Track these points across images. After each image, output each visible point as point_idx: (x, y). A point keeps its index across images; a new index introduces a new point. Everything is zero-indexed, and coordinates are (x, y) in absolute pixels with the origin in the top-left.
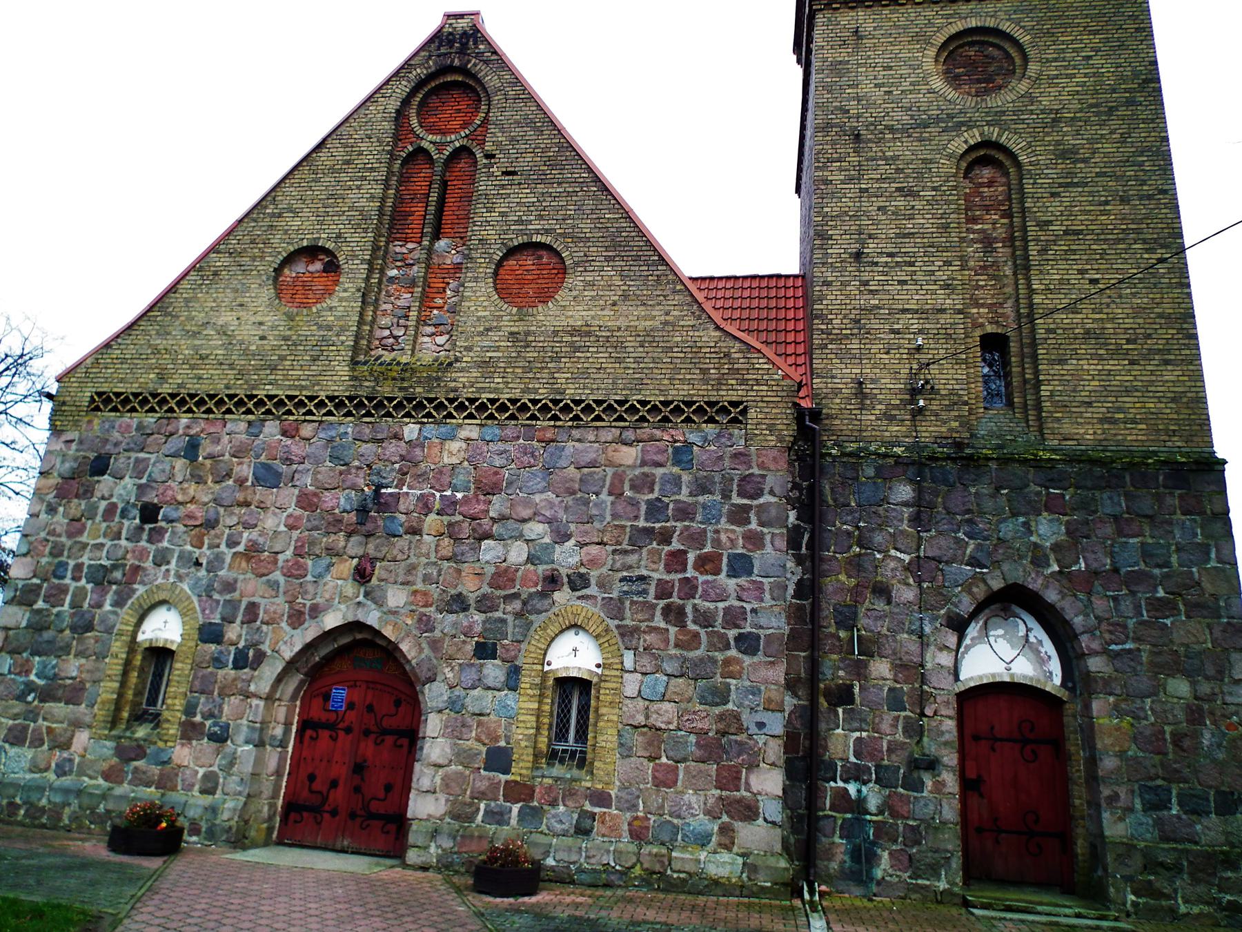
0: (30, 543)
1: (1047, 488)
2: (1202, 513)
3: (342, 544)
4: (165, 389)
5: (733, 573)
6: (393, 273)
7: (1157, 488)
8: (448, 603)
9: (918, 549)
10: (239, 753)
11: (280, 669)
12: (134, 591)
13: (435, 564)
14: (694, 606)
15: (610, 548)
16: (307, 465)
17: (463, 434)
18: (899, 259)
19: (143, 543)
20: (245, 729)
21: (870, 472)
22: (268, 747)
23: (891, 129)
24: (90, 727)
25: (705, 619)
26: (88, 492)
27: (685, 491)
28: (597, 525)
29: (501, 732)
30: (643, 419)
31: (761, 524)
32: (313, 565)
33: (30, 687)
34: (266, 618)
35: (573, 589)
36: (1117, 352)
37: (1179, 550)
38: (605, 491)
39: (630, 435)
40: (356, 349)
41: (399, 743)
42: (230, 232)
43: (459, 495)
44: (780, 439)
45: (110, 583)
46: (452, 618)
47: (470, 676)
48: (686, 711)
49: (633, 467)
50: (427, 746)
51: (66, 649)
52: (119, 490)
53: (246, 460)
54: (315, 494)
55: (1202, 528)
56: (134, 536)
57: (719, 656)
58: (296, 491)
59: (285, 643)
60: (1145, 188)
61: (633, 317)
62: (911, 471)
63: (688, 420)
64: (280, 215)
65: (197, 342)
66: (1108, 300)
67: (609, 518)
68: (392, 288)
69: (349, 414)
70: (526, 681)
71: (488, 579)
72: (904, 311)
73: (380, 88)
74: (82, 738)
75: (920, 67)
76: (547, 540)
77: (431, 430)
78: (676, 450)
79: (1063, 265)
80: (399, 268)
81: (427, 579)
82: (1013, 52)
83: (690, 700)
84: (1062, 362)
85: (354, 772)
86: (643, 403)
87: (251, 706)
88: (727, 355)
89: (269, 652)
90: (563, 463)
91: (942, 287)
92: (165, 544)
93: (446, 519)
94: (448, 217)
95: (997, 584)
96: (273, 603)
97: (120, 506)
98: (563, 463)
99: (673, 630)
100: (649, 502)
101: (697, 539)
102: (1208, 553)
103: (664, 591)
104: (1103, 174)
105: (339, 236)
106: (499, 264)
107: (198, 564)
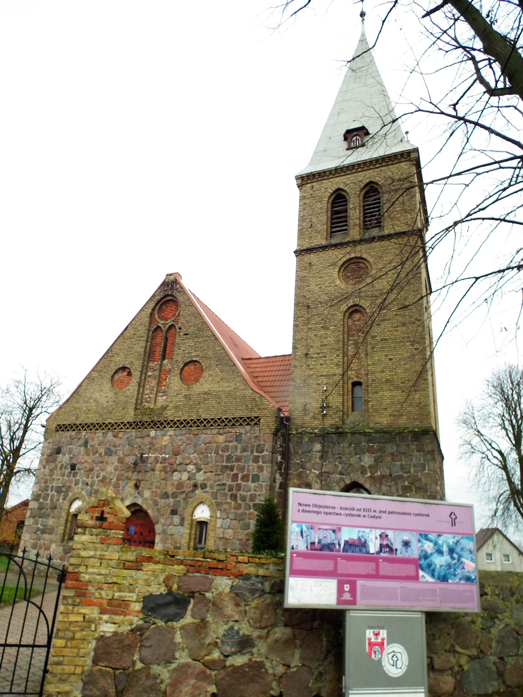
0: (38, 479)
1: (368, 443)
2: (424, 451)
3: (131, 475)
4: (78, 422)
5: (253, 482)
6: (150, 374)
7: (408, 442)
8: (163, 495)
9: (322, 468)
12: (68, 495)
13: (159, 481)
14: (240, 494)
15: (214, 474)
16: (121, 447)
17: (169, 433)
18: (321, 355)
19: (71, 478)
21: (306, 439)
23: (321, 303)
24: (56, 542)
25: (243, 499)
26: (55, 461)
27: (239, 451)
28: (210, 465)
29: (178, 541)
30: (226, 425)
31: (263, 462)
33: (38, 529)
35: (202, 489)
36: (397, 388)
37: (414, 466)
38: (213, 452)
39: (222, 431)
40: (136, 404)
42: (98, 364)
43: (167, 456)
44: (271, 430)
45: (62, 492)
46: (164, 501)
47: (169, 521)
48: (236, 532)
49: (222, 443)
51: (49, 516)
52: (64, 459)
53: (102, 447)
54: (123, 458)
55: (423, 457)
56: (68, 476)
57: (247, 512)
58: (117, 457)
60: (412, 319)
61: (226, 387)
62: (321, 438)
63: (241, 424)
64: (113, 356)
65: (88, 405)
66: (395, 367)
67: (214, 462)
68: (150, 379)
69: (134, 428)
70: (187, 523)
71: (175, 486)
72: (322, 376)
73: (145, 305)
74: (53, 546)
75: (332, 276)
76: (194, 471)
77: (159, 433)
78: (237, 436)
79: (379, 353)
80: (152, 372)
81: (157, 487)
82: (368, 265)
83: (237, 528)
84: (377, 393)
86: (226, 419)
88: (254, 399)
90: (200, 443)
91: (336, 366)
92: (78, 478)
93: (163, 465)
94: (167, 352)
95: (348, 482)
97: (65, 465)
98: (200, 443)
99: (233, 503)
100: (227, 456)
101: (242, 469)
102: (425, 467)
103: (231, 489)
104: (396, 315)
105: (131, 362)
106: (182, 369)
107: (87, 484)
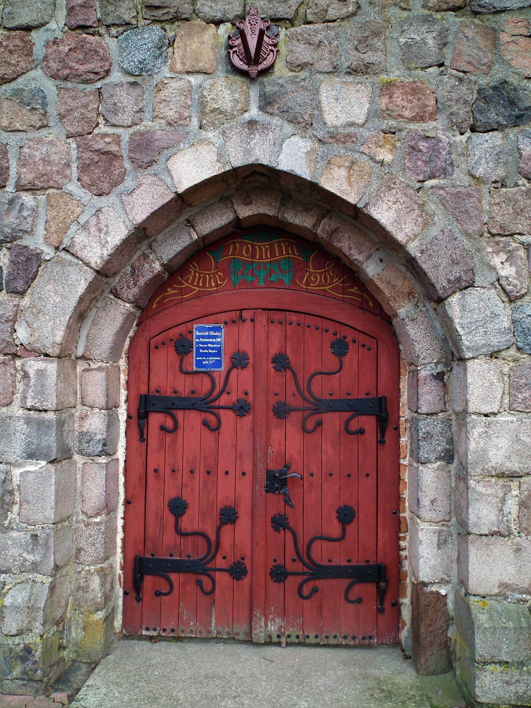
10: (16, 480)
11: (81, 287)
20: (21, 426)
22: (76, 457)
32: (122, 50)
34: (28, 176)
41: (354, 425)
50: (476, 433)
59: (85, 227)
85: (269, 489)
87: (26, 375)
89: (48, 252)
96: (39, 141)
